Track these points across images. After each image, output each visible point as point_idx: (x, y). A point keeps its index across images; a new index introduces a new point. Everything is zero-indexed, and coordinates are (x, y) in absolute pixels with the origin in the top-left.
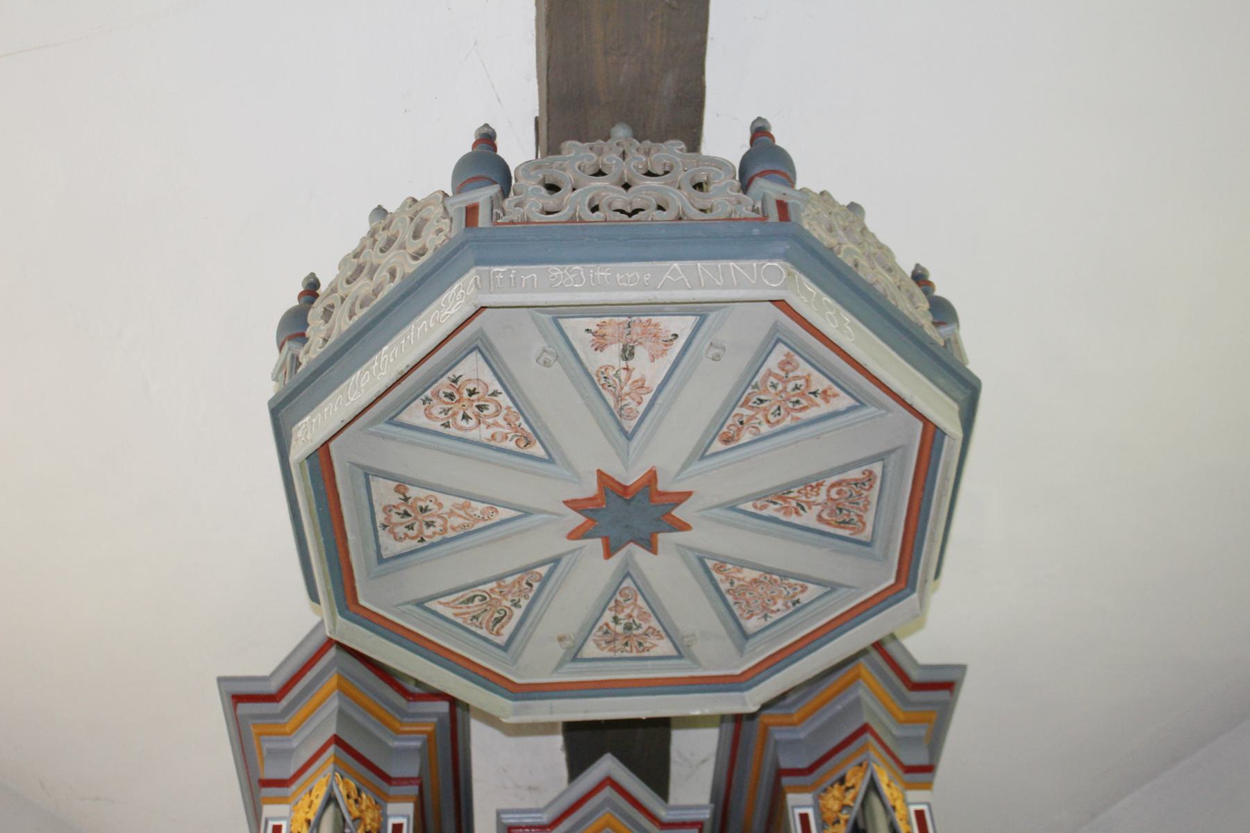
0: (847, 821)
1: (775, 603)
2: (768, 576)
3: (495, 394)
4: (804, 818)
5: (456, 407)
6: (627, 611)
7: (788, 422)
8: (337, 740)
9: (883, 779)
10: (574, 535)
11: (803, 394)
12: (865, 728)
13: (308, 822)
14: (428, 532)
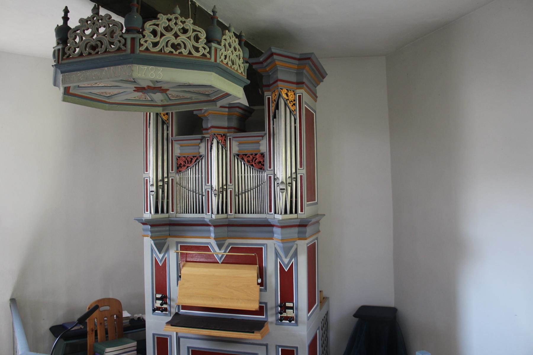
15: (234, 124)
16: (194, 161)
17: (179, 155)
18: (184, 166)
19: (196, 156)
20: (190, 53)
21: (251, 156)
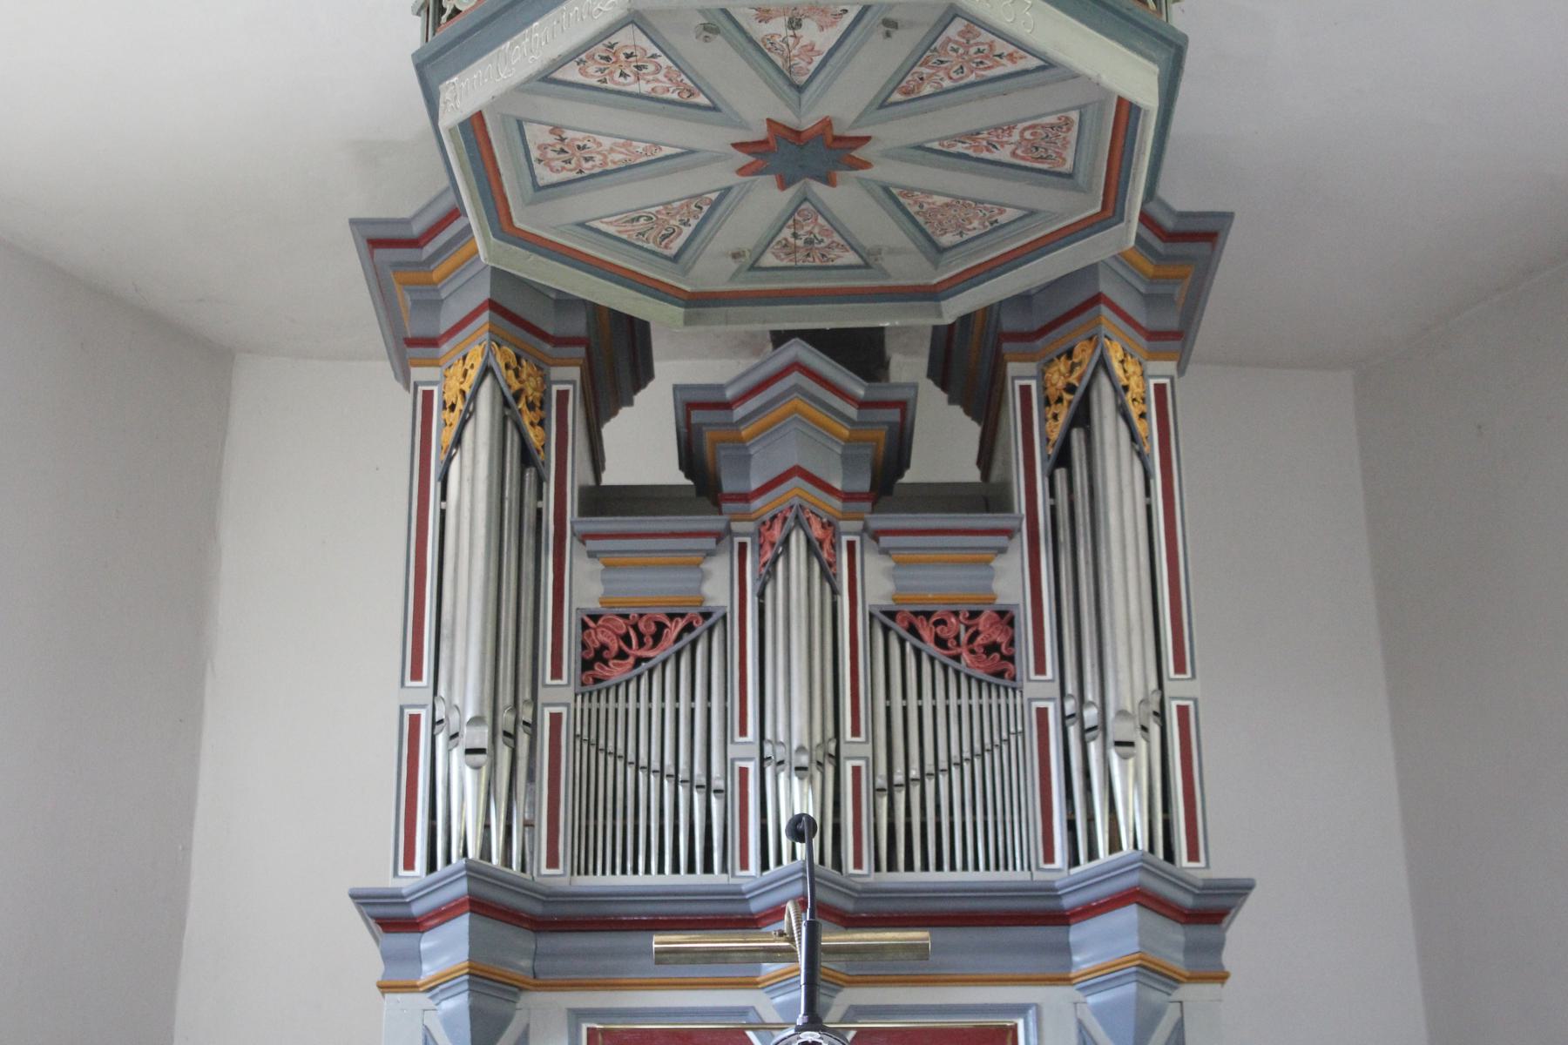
0: (1070, 402)
1: (971, 223)
3: (654, 56)
4: (1026, 391)
6: (807, 228)
7: (972, 78)
8: (492, 305)
9: (1115, 355)
10: (742, 171)
11: (987, 57)
12: (1098, 299)
13: (463, 393)
15: (863, 484)
16: (674, 629)
17: (595, 606)
18: (622, 655)
19: (682, 616)
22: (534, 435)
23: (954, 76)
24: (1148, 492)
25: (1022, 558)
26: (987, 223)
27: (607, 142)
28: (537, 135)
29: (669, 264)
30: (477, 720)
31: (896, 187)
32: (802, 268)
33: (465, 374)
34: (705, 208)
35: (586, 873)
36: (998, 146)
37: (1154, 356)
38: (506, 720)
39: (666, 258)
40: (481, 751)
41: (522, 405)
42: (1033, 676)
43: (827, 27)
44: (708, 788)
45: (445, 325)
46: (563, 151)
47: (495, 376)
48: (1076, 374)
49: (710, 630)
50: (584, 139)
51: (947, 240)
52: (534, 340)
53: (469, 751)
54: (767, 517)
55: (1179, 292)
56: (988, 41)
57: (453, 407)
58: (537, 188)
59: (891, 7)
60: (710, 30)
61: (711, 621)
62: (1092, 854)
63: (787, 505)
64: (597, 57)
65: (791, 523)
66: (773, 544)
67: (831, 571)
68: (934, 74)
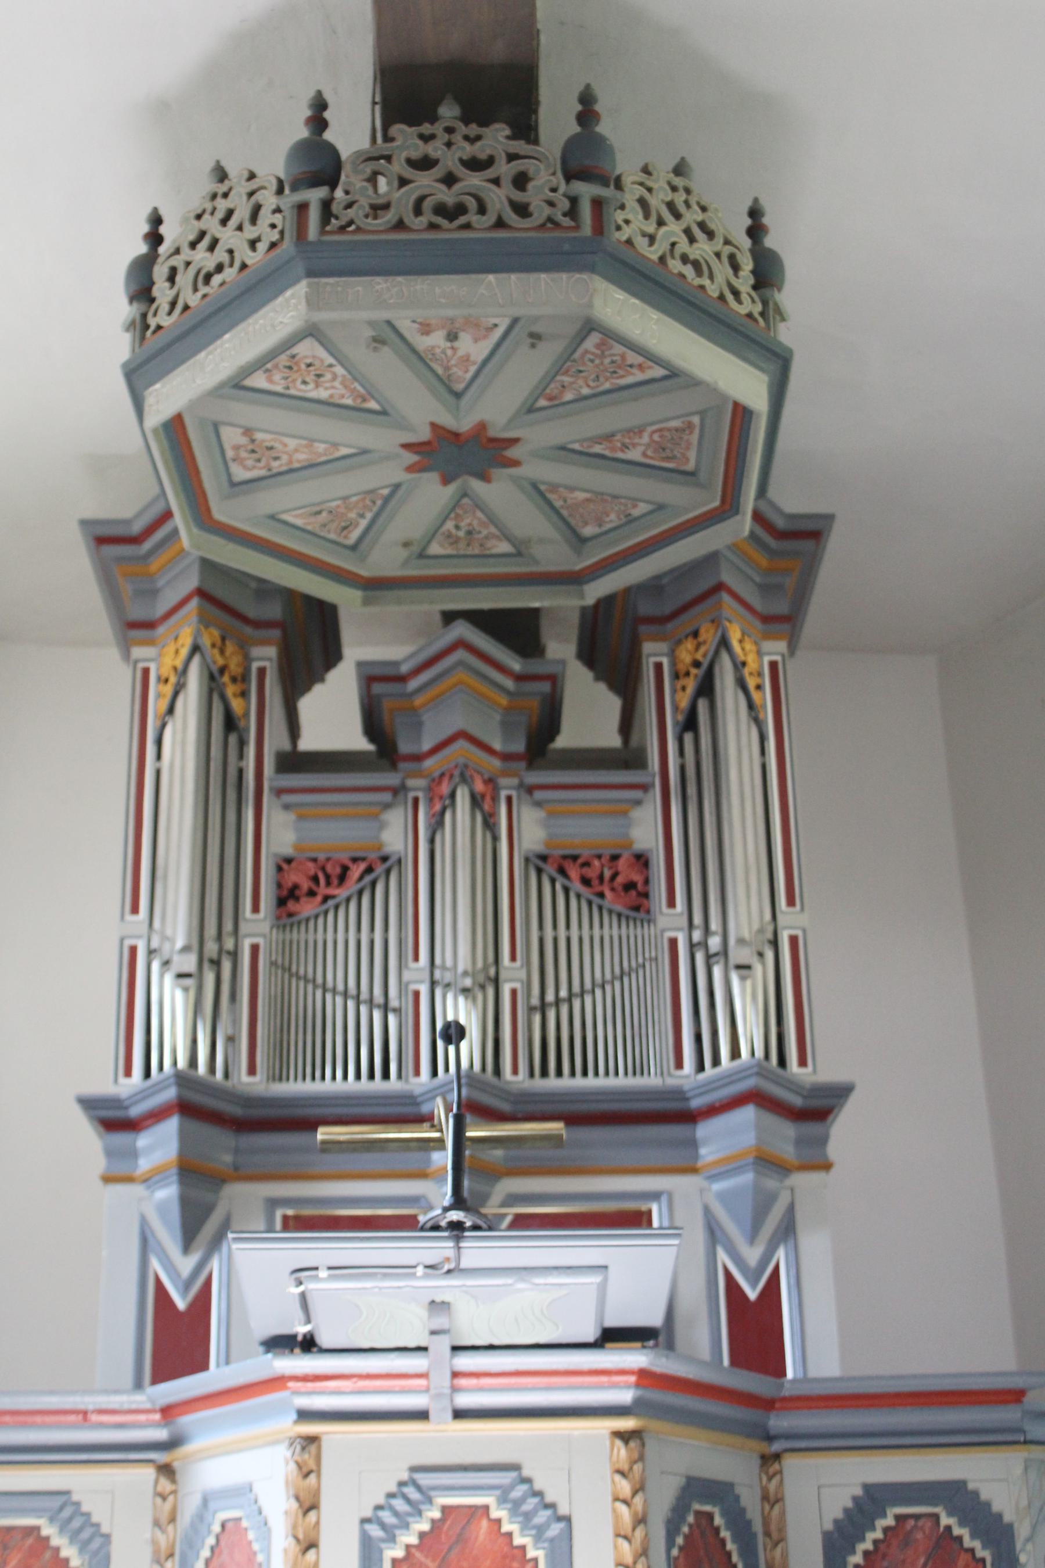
0: (696, 676)
1: (608, 516)
2: (599, 497)
3: (331, 366)
4: (659, 667)
5: (295, 376)
6: (468, 521)
7: (607, 386)
8: (201, 593)
9: (735, 636)
10: (410, 469)
11: (620, 367)
12: (720, 587)
13: (175, 669)
14: (275, 464)
15: (519, 746)
16: (356, 871)
17: (288, 851)
18: (312, 893)
19: (363, 859)
20: (722, 297)
21: (596, 863)
22: (237, 705)
23: (591, 384)
24: (763, 752)
25: (655, 808)
26: (622, 517)
27: (292, 443)
28: (231, 436)
29: (347, 552)
30: (186, 949)
31: (544, 483)
32: (465, 556)
33: (177, 652)
34: (379, 502)
35: (280, 1079)
36: (630, 447)
37: (767, 636)
38: (211, 948)
39: (345, 547)
40: (188, 975)
41: (226, 679)
42: (665, 909)
43: (480, 339)
44: (385, 1008)
45: (161, 609)
46: (253, 451)
47: (203, 656)
48: (703, 649)
49: (388, 872)
50: (272, 440)
51: (588, 531)
52: (238, 624)
53: (181, 976)
54: (437, 774)
55: (789, 582)
56: (620, 352)
57: (166, 681)
58: (233, 484)
59: (536, 319)
60: (378, 341)
61: (388, 864)
62: (716, 1061)
63: (452, 765)
64: (281, 366)
65: (457, 779)
66: (441, 798)
67: (492, 821)
68: (574, 383)
